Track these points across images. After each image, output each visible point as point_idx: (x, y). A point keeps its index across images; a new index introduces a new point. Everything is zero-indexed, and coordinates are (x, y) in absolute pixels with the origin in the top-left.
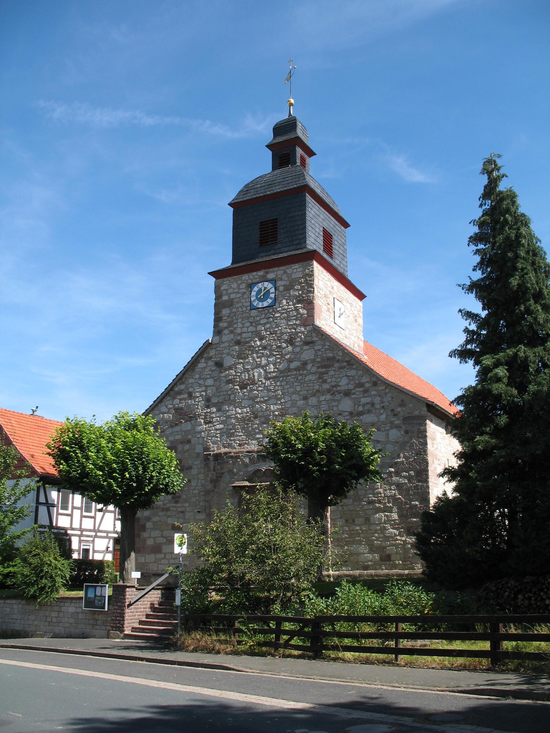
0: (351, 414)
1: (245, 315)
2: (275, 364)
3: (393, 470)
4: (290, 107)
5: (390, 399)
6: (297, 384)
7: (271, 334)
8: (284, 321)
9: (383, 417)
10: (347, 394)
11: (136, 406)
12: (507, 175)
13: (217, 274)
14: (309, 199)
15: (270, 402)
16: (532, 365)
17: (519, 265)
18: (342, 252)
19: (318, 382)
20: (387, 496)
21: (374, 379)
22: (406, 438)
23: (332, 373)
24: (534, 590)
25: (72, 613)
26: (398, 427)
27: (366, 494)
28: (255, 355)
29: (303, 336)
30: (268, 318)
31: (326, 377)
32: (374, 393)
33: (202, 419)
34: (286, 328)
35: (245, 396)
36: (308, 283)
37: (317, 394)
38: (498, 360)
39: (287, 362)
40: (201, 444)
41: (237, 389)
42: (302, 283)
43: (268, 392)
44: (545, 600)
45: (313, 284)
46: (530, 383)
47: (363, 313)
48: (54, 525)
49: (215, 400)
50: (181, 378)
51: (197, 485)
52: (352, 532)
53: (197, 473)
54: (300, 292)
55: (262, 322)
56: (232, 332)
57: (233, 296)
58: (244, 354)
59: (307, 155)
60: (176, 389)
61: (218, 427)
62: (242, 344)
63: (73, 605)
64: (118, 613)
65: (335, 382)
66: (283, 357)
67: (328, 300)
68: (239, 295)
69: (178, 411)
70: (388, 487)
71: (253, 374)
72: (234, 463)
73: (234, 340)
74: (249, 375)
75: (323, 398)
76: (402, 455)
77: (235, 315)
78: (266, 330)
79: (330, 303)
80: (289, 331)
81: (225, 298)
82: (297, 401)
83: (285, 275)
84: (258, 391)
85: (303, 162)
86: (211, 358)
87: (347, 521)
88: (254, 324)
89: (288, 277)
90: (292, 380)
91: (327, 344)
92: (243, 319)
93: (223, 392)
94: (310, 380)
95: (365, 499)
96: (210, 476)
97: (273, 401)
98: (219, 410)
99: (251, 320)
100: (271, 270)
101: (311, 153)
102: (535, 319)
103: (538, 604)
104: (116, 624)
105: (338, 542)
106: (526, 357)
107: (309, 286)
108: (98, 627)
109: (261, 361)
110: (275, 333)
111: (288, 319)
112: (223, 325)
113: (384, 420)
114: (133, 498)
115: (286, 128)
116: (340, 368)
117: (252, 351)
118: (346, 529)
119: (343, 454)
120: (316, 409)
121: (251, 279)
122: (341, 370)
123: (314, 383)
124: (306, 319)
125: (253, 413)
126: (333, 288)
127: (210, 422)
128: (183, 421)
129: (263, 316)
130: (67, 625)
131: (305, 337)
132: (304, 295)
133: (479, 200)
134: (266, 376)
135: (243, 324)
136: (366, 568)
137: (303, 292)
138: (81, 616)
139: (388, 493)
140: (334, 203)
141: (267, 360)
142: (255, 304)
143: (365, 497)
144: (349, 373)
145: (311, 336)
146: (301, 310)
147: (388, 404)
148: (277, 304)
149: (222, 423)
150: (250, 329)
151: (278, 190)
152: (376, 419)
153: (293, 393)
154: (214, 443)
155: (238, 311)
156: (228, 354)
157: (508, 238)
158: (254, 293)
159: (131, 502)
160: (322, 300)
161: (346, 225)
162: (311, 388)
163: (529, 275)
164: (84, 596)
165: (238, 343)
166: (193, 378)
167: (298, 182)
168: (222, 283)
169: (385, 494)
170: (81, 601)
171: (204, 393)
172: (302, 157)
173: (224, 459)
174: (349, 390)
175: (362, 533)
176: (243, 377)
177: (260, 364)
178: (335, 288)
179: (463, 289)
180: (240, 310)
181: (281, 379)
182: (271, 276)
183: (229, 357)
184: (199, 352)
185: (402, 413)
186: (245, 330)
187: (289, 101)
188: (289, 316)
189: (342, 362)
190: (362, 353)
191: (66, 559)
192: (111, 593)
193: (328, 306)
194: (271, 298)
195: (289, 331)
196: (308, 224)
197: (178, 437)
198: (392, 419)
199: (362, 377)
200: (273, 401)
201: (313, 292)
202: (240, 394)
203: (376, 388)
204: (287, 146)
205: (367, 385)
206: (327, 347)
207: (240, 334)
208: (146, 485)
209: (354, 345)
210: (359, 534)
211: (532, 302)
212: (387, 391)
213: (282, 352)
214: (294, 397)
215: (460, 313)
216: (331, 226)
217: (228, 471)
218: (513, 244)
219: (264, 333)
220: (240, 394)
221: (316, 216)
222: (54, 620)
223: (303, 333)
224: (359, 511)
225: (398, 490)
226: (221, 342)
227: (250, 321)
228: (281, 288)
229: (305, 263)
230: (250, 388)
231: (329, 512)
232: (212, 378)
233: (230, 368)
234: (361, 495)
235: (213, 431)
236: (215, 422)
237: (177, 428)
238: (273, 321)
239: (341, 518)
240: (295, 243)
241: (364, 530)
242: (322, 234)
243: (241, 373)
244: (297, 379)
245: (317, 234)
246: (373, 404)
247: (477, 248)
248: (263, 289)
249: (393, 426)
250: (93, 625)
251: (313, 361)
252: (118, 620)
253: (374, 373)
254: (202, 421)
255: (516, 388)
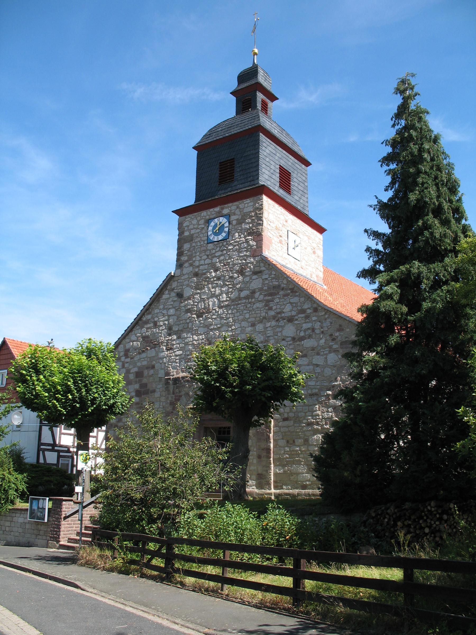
0: (293, 339)
1: (202, 249)
2: (227, 294)
3: (330, 392)
4: (254, 56)
5: (329, 324)
6: (246, 311)
7: (225, 265)
8: (236, 253)
9: (322, 341)
10: (290, 320)
11: (107, 334)
12: (419, 93)
13: (181, 212)
14: (262, 137)
15: (222, 329)
16: (425, 281)
17: (420, 180)
18: (302, 189)
19: (265, 309)
20: (324, 418)
21: (315, 305)
22: (343, 362)
23: (277, 300)
24: (413, 517)
25: (21, 523)
26: (336, 351)
27: (306, 416)
28: (210, 286)
29: (252, 267)
30: (222, 251)
31: (271, 304)
32: (314, 318)
33: (164, 346)
34: (237, 260)
35: (201, 324)
36: (257, 216)
37: (264, 320)
38: (392, 277)
39: (238, 292)
40: (163, 369)
41: (194, 318)
42: (252, 216)
43: (221, 320)
44: (424, 528)
45: (262, 217)
46: (424, 300)
47: (323, 246)
48: (57, 443)
49: (175, 328)
50: (148, 309)
51: (159, 408)
52: (293, 453)
53: (159, 396)
54: (251, 225)
55: (217, 255)
56: (191, 265)
57: (193, 232)
58: (201, 284)
59: (269, 100)
60: (144, 319)
61: (178, 353)
62: (199, 276)
63: (22, 515)
64: (56, 524)
65: (280, 309)
66: (234, 287)
67: (281, 232)
68: (198, 230)
69: (145, 338)
70: (325, 409)
71: (208, 303)
72: (190, 387)
73: (193, 272)
74: (205, 304)
75: (268, 325)
76: (339, 378)
77: (194, 249)
78: (220, 262)
79: (283, 235)
80: (240, 262)
81: (186, 234)
82: (246, 327)
83: (238, 210)
84: (212, 319)
85: (265, 108)
86: (173, 289)
87: (288, 442)
88: (210, 257)
89: (241, 212)
90: (242, 308)
91: (273, 273)
92: (201, 252)
93: (182, 320)
94: (258, 308)
95: (305, 421)
96: (170, 398)
97: (225, 328)
98: (179, 338)
99: (208, 253)
100: (226, 206)
101: (273, 98)
102: (432, 234)
103: (418, 532)
104: (54, 534)
105: (280, 462)
106: (419, 274)
107: (258, 218)
108: (40, 537)
109: (215, 291)
110: (228, 264)
111: (239, 251)
112: (184, 258)
113: (324, 344)
114: (77, 418)
115: (248, 76)
116: (284, 296)
117: (208, 282)
118: (287, 449)
119: (259, 376)
120: (262, 335)
121: (209, 215)
122: (285, 298)
123: (261, 311)
124: (255, 250)
125: (208, 340)
126: (286, 221)
127: (171, 349)
128: (149, 348)
129: (218, 248)
130: (17, 534)
131: (254, 268)
132: (254, 228)
133: (392, 120)
134: (220, 304)
135: (201, 257)
136: (304, 487)
137: (253, 225)
138: (28, 526)
139: (326, 415)
140: (294, 143)
141: (221, 290)
142: (211, 238)
143: (304, 419)
144: (292, 301)
145: (259, 266)
146: (251, 242)
147: (327, 329)
148: (230, 237)
149: (181, 349)
150: (206, 262)
151: (236, 132)
152: (315, 344)
153: (243, 320)
154: (174, 368)
155: (197, 246)
156: (188, 285)
157: (412, 154)
158: (210, 228)
159: (76, 422)
160: (273, 233)
161: (307, 163)
162: (259, 315)
163: (428, 190)
164: (29, 508)
165: (196, 275)
166: (158, 308)
167: (253, 123)
168: (185, 220)
169: (322, 416)
170: (26, 512)
171: (166, 322)
172: (263, 101)
173: (181, 383)
174: (293, 316)
175: (301, 453)
176: (200, 306)
177: (214, 294)
178: (290, 222)
179: (374, 209)
180: (199, 244)
181: (233, 307)
182: (226, 211)
183: (188, 288)
184: (163, 285)
185: (339, 337)
186: (202, 262)
187: (253, 51)
188: (240, 248)
189: (286, 289)
190: (321, 283)
191: (19, 473)
192: (50, 506)
193: (281, 238)
194: (225, 232)
195: (240, 262)
196: (261, 161)
197: (145, 363)
198: (331, 344)
199: (304, 303)
200: (225, 328)
201: (262, 225)
202: (197, 322)
203: (317, 314)
204: (249, 92)
205: (309, 311)
206: (273, 276)
207: (198, 267)
208: (89, 407)
209: (311, 275)
210: (299, 454)
211: (431, 215)
212: (326, 316)
213: (233, 282)
214: (244, 324)
215: (366, 234)
216: (290, 164)
217: (185, 394)
218: (417, 160)
219: (218, 265)
220: (197, 322)
221: (272, 154)
222: (7, 529)
223: (252, 263)
224: (299, 432)
225: (335, 412)
226: (182, 275)
227: (206, 254)
228: (234, 222)
229: (255, 198)
230: (205, 316)
231: (272, 433)
232: (174, 308)
233: (189, 298)
234: (301, 417)
235: (173, 357)
236: (176, 348)
237: (144, 355)
238: (227, 253)
239: (283, 439)
240: (249, 179)
241: (303, 451)
242: (278, 171)
243: (198, 303)
244: (246, 307)
245: (272, 171)
246: (313, 330)
247: (389, 168)
248: (218, 224)
249: (332, 350)
250: (37, 535)
251: (261, 290)
252: (55, 531)
253: (314, 299)
254: (165, 348)
255: (406, 306)
